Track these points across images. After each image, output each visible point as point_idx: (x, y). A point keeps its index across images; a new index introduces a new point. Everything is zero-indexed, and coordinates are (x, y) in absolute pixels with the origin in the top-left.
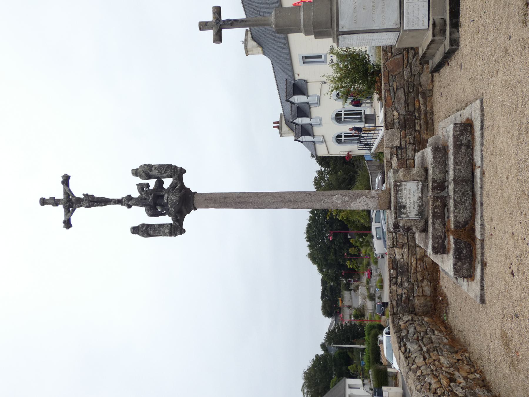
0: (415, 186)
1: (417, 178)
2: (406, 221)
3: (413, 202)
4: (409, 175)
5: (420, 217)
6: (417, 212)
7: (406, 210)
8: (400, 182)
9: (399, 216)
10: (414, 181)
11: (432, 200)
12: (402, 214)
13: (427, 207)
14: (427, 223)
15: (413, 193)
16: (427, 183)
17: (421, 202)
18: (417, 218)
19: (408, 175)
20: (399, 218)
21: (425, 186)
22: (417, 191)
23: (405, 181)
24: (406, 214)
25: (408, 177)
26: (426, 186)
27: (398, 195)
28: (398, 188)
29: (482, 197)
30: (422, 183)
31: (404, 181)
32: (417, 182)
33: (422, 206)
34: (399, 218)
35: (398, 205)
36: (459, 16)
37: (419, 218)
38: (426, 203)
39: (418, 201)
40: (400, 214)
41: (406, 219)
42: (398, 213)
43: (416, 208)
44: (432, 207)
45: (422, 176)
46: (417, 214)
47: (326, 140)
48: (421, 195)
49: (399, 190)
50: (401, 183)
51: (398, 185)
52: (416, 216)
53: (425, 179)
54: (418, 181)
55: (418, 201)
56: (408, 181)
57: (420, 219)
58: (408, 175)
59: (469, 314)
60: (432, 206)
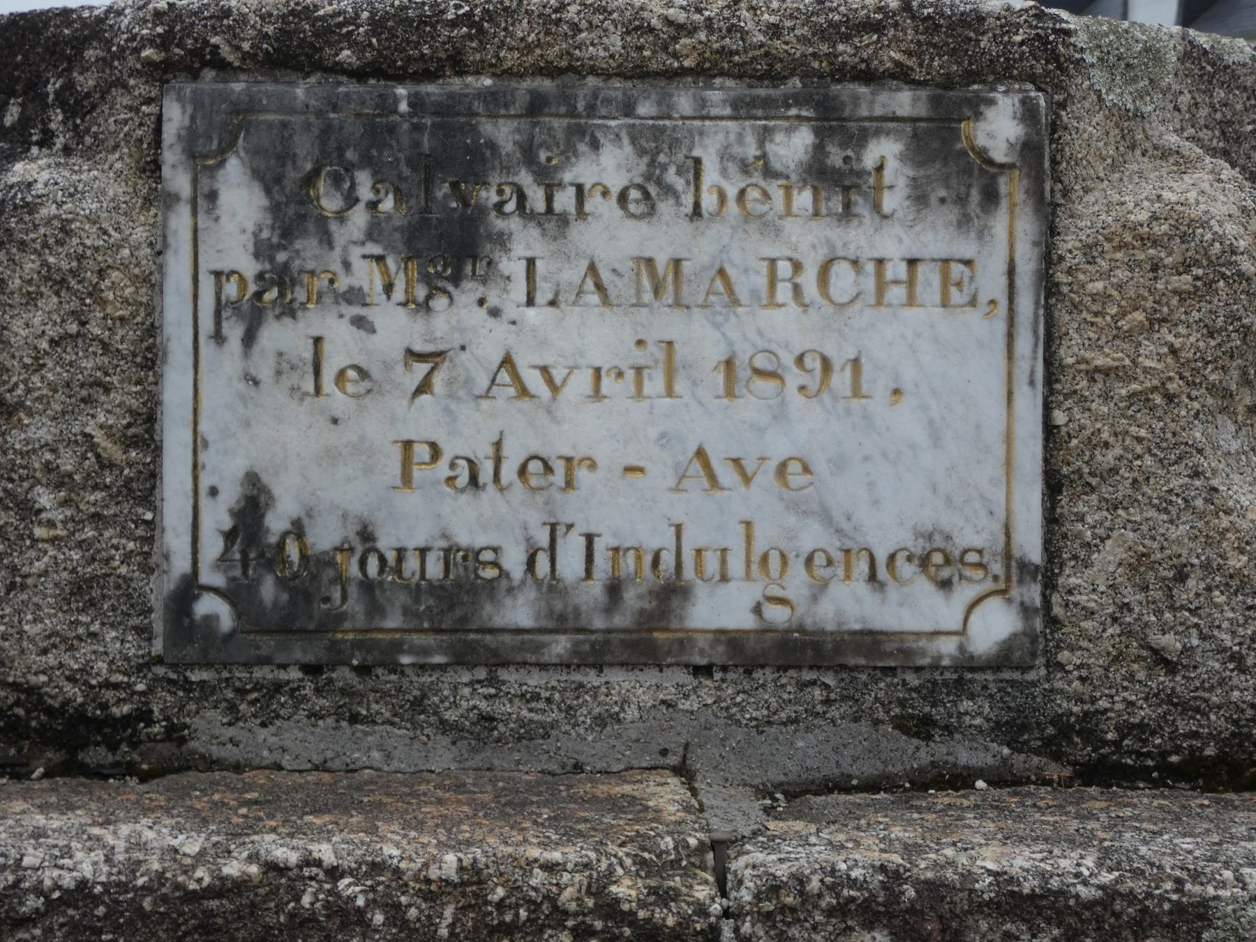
0: (930, 514)
1: (1110, 555)
2: (118, 287)
3: (558, 444)
4: (1192, 375)
5: (208, 605)
6: (324, 537)
7: (365, 276)
8: (1029, 149)
9: (244, 111)
10: (1053, 484)
11: (625, 889)
12: (268, 180)
13: (443, 756)
14: (70, 768)
15: (779, 448)
16: (1002, 778)
17: (562, 622)
18: (176, 540)
19: (1190, 340)
20: (175, 117)
21: (921, 728)
22: (812, 536)
23: (1048, 287)
24: (282, 278)
25: (1150, 355)
26: (918, 754)
27: (742, 109)
28: (904, 101)
29: (669, 78)
30: (1003, 659)
31: (1048, 258)
32: (1030, 544)
33: (463, 657)
34: (175, 117)
35: (495, 102)
36: (178, 587)
37: (189, 588)
38: (526, 734)
39: (571, 562)
40: (285, 156)
41: (152, 282)
42: (301, 91)
43: (410, 502)
44: (433, 892)
45: (1160, 659)
46: (276, 523)
47: (944, 256)
48: (732, 640)
49: (860, 139)
50: (1013, 188)
51: (976, 108)
52: (216, 517)
53: (1088, 726)
54: (1050, 584)
55: (571, 562)
56: (1051, 339)
57: (159, 590)
58: (1190, 340)
59: (617, 709)
60: (473, 877)
